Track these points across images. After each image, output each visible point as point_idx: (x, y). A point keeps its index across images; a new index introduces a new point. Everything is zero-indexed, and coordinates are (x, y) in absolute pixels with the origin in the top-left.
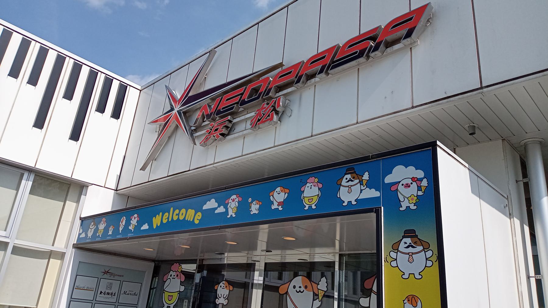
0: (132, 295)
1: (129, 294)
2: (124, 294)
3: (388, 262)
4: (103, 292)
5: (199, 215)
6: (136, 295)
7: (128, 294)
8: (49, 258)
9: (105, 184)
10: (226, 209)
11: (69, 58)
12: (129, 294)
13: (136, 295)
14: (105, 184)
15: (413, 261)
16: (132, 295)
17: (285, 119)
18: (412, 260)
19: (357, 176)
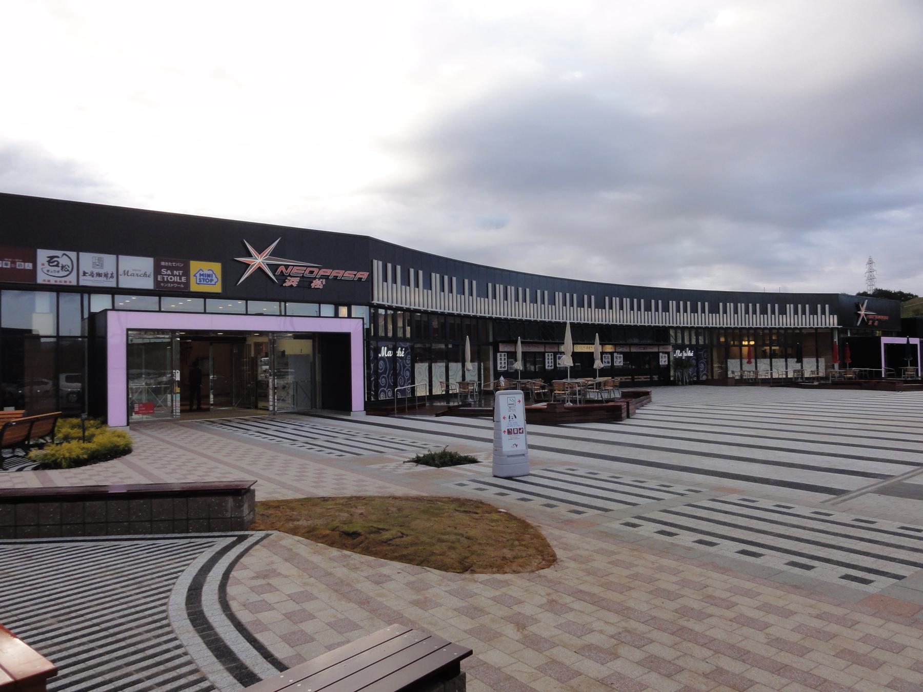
7: (133, 275)
12: (134, 276)
13: (149, 277)
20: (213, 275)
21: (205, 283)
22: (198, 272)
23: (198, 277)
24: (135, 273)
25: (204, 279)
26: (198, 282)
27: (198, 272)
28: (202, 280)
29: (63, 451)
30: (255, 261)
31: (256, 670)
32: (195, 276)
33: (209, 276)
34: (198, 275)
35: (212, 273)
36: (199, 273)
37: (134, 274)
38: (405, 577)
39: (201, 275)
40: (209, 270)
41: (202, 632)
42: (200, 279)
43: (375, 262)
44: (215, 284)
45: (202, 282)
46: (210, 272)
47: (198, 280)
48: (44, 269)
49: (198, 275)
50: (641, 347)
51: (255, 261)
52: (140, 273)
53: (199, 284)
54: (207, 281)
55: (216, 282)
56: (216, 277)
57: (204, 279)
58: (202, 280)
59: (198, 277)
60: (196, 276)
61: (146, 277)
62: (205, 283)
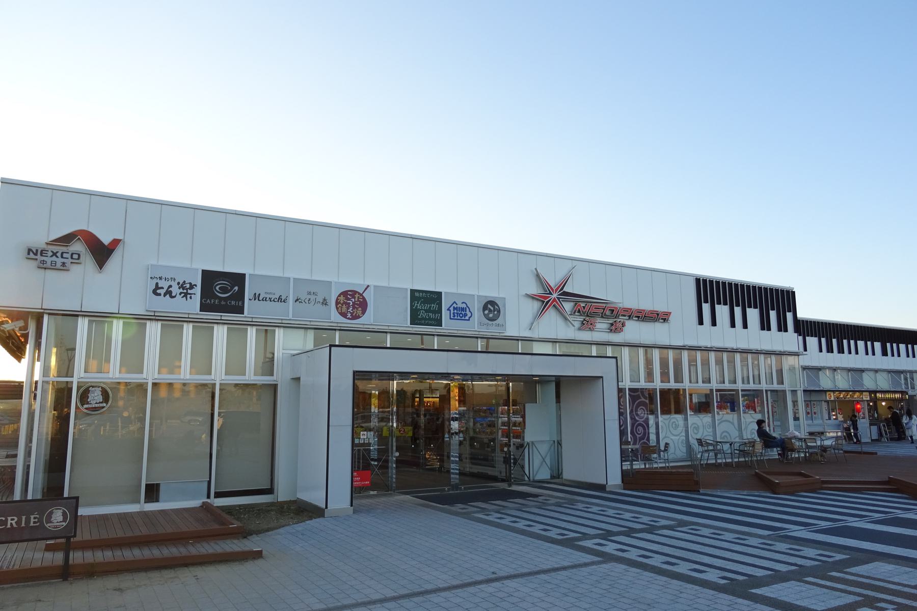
0: (274, 301)
1: (266, 300)
2: (255, 299)
3: (68, 258)
4: (162, 288)
5: (448, 439)
6: (284, 301)
7: (265, 299)
8: (38, 345)
9: (90, 199)
10: (126, 417)
11: (871, 374)
12: (266, 300)
13: (284, 301)
14: (90, 199)
15: (44, 252)
16: (274, 301)
17: (638, 322)
18: (719, 362)
19: (536, 474)
20: (467, 309)
21: (459, 318)
22: (452, 304)
23: (452, 312)
24: (268, 296)
25: (457, 313)
26: (452, 317)
27: (452, 304)
28: (456, 315)
29: (375, 422)
30: (549, 297)
31: (499, 446)
32: (449, 309)
33: (463, 309)
34: (452, 309)
35: (466, 306)
36: (452, 307)
37: (266, 298)
38: (108, 589)
39: (454, 308)
40: (462, 303)
41: (632, 392)
42: (454, 313)
43: (887, 344)
44: (469, 320)
45: (456, 318)
46: (464, 306)
47: (452, 315)
48: (455, 304)
49: (452, 309)
50: (145, 531)
51: (549, 297)
52: (273, 297)
53: (452, 319)
54: (461, 315)
55: (469, 318)
56: (470, 311)
57: (457, 313)
58: (456, 315)
59: (452, 312)
60: (450, 310)
61: (281, 302)
62: (459, 318)
